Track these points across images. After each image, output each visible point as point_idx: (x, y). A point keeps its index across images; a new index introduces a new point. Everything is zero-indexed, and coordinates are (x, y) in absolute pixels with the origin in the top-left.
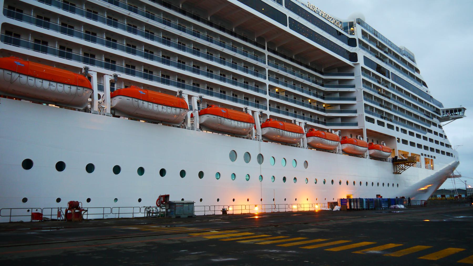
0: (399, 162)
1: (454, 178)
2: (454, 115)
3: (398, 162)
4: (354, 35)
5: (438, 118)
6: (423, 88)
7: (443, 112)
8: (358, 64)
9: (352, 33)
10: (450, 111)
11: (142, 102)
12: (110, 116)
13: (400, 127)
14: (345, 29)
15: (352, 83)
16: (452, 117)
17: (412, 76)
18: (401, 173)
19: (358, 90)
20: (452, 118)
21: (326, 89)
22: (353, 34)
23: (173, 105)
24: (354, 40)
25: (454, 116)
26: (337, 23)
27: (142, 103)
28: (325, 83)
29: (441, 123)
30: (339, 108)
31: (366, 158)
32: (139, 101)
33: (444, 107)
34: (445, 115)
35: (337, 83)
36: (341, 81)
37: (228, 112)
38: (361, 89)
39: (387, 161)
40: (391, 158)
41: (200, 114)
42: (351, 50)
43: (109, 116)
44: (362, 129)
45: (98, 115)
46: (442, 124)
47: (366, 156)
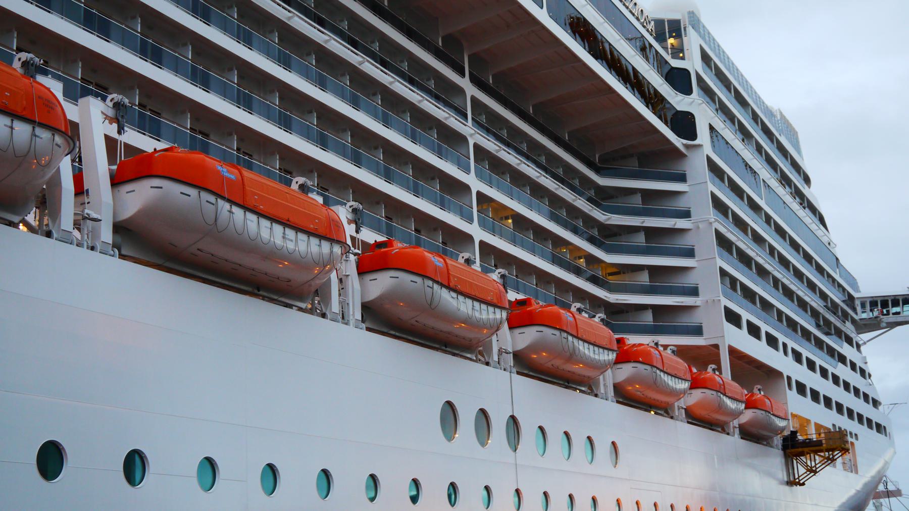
0: (802, 447)
1: (889, 498)
2: (891, 315)
3: (800, 450)
4: (683, 58)
5: (854, 322)
6: (820, 231)
7: (863, 305)
8: (700, 146)
9: (678, 52)
10: (882, 301)
11: (227, 206)
12: (110, 255)
13: (791, 344)
14: (660, 37)
15: (681, 204)
16: (886, 319)
17: (798, 194)
18: (803, 484)
19: (701, 226)
20: (887, 323)
21: (609, 219)
22: (681, 55)
23: (312, 226)
24: (685, 73)
25: (891, 319)
26: (645, 20)
27: (228, 213)
28: (602, 197)
29: (861, 336)
30: (644, 278)
31: (733, 435)
32: (221, 202)
33: (860, 292)
34: (868, 315)
35: (637, 201)
36: (648, 195)
37: (450, 267)
38: (711, 223)
39: (772, 447)
40: (809, 437)
41: (362, 270)
42: (678, 103)
43: (106, 254)
44: (716, 346)
45: (74, 247)
46: (865, 337)
47: (734, 430)
